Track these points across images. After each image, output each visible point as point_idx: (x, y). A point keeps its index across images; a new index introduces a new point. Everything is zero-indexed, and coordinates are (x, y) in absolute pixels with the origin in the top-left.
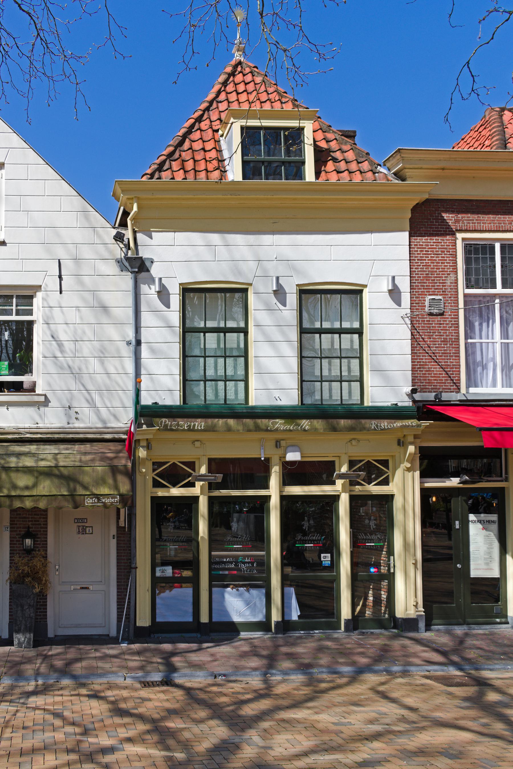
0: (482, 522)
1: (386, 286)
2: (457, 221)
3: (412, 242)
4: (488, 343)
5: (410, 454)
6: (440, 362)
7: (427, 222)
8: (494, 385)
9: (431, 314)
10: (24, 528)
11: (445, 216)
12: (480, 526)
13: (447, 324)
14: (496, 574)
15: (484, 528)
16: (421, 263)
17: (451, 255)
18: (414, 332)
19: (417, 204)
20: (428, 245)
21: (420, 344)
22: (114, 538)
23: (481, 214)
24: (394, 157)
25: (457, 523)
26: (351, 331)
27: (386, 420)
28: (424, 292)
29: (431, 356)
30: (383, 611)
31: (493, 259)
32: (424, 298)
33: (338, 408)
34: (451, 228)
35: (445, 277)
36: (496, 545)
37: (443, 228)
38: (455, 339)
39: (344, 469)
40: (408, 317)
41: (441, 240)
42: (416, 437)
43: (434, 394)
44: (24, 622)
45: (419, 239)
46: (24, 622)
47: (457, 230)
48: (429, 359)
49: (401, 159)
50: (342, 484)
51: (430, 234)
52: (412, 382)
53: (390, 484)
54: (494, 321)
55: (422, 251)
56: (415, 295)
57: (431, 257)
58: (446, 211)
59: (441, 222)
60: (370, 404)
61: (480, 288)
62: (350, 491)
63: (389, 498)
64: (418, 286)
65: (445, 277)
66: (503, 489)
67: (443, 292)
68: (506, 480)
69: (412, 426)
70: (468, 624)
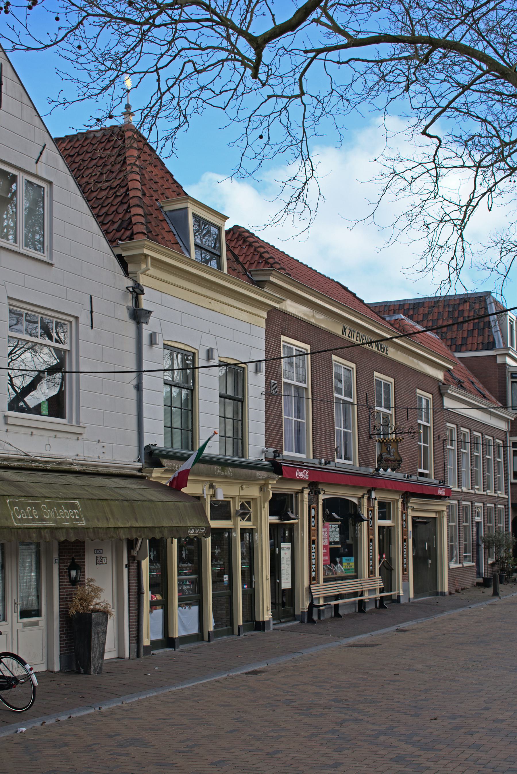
10: (69, 559)
22: (126, 567)
44: (98, 649)
46: (98, 649)
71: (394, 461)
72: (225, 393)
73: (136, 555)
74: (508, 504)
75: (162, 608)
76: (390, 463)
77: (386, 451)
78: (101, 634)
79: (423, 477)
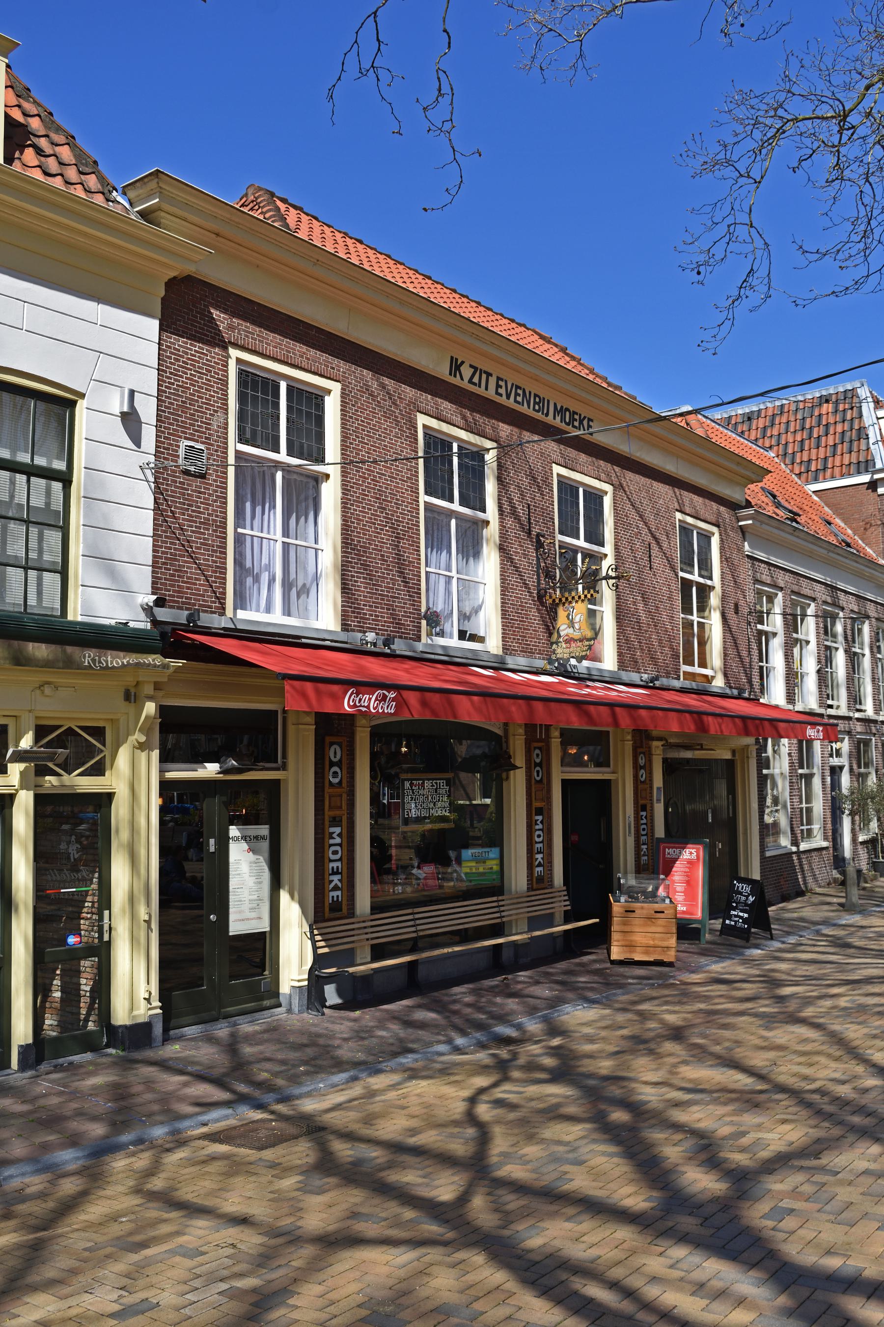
0: (248, 839)
1: (117, 404)
2: (231, 327)
3: (164, 340)
4: (262, 538)
5: (147, 717)
6: (197, 558)
7: (188, 314)
8: (268, 609)
9: (186, 472)
11: (215, 313)
12: (245, 846)
13: (210, 495)
14: (264, 926)
15: (251, 850)
16: (176, 380)
17: (220, 379)
18: (159, 499)
19: (175, 278)
20: (187, 353)
21: (167, 522)
23: (265, 329)
24: (145, 184)
25: (212, 841)
26: (48, 474)
27: (109, 652)
28: (177, 431)
29: (183, 546)
30: (82, 1017)
31: (277, 405)
32: (178, 441)
33: (23, 618)
34: (223, 337)
35: (210, 414)
36: (266, 875)
37: (211, 332)
38: (220, 522)
39: (26, 742)
40: (151, 469)
41: (207, 350)
42: (157, 686)
43: (186, 613)
45: (175, 339)
47: (230, 342)
48: (180, 550)
49: (158, 189)
50: (21, 773)
51: (191, 335)
52: (153, 588)
53: (107, 773)
54: (273, 506)
55: (178, 360)
56: (163, 432)
57: (191, 374)
58: (217, 308)
59: (208, 321)
60: (80, 619)
61: (258, 447)
62: (36, 786)
63: (105, 799)
64: (169, 418)
65: (210, 414)
66: (277, 782)
67: (206, 438)
68: (284, 767)
69: (155, 666)
70: (227, 1017)
71: (581, 640)
72: (29, 461)
76: (573, 645)
77: (567, 622)
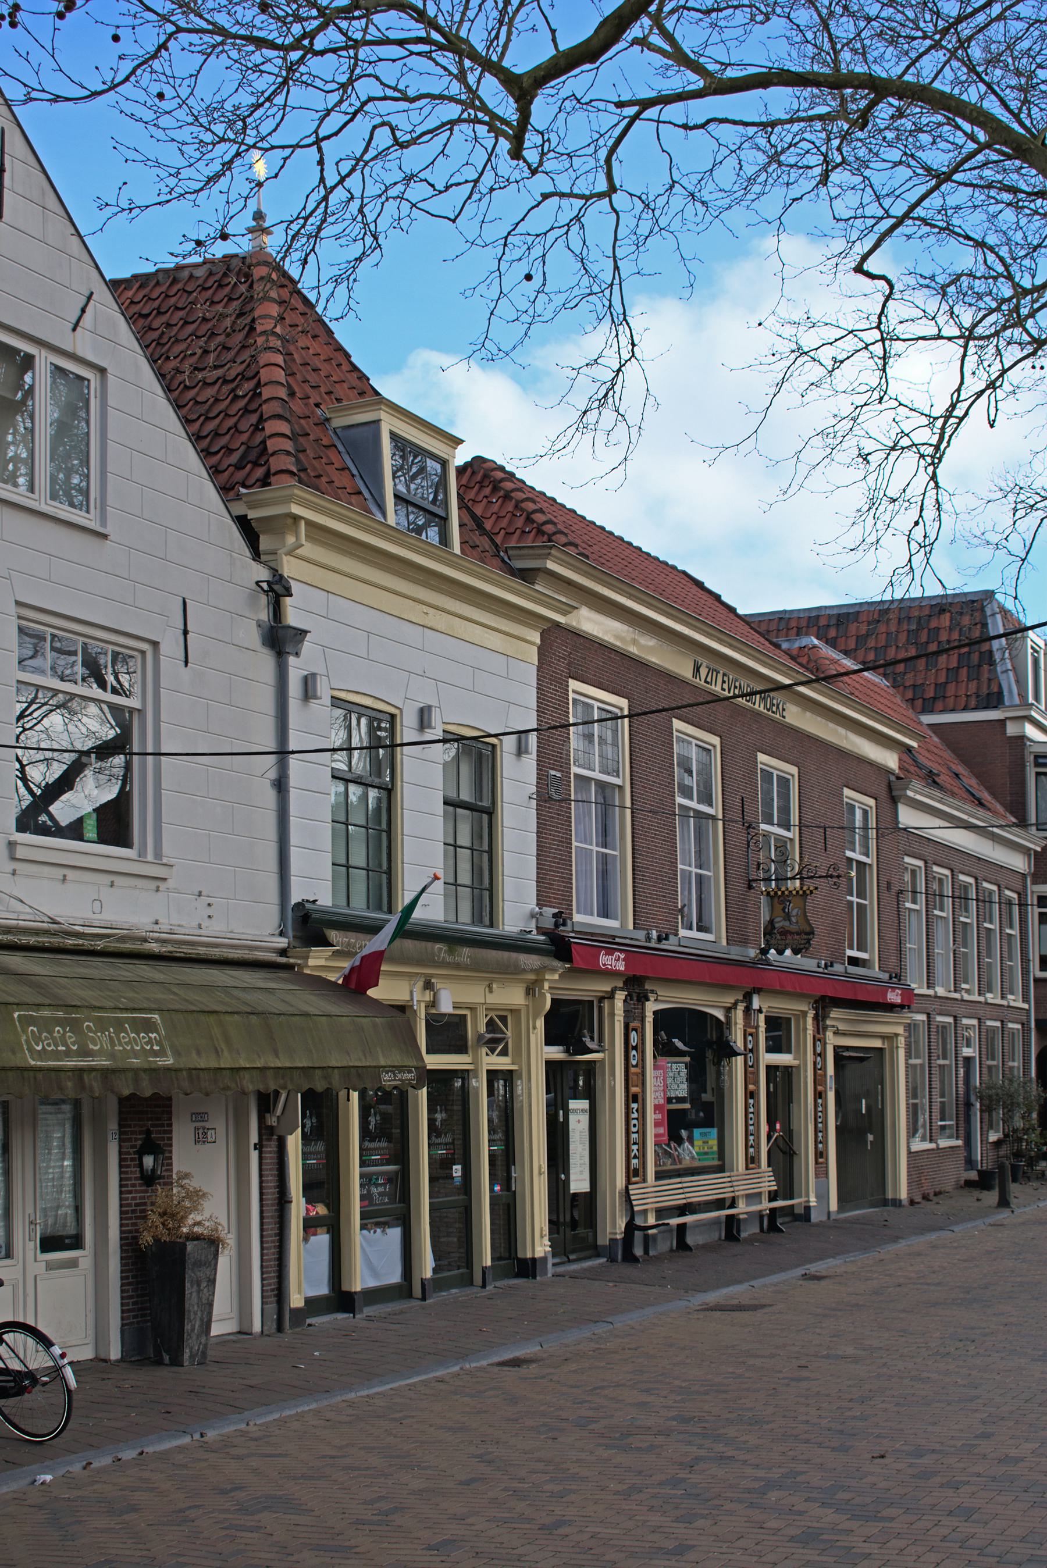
10: (140, 1133)
22: (255, 1148)
44: (199, 1314)
46: (199, 1314)
71: (798, 934)
72: (455, 795)
73: (275, 1124)
74: (1029, 1022)
75: (328, 1232)
76: (789, 937)
77: (783, 914)
78: (204, 1284)
79: (857, 966)
